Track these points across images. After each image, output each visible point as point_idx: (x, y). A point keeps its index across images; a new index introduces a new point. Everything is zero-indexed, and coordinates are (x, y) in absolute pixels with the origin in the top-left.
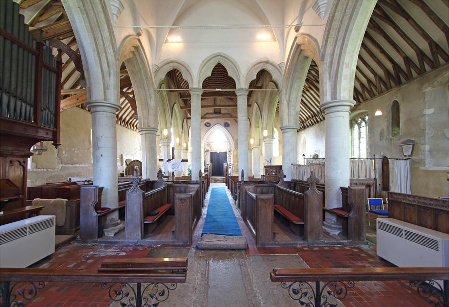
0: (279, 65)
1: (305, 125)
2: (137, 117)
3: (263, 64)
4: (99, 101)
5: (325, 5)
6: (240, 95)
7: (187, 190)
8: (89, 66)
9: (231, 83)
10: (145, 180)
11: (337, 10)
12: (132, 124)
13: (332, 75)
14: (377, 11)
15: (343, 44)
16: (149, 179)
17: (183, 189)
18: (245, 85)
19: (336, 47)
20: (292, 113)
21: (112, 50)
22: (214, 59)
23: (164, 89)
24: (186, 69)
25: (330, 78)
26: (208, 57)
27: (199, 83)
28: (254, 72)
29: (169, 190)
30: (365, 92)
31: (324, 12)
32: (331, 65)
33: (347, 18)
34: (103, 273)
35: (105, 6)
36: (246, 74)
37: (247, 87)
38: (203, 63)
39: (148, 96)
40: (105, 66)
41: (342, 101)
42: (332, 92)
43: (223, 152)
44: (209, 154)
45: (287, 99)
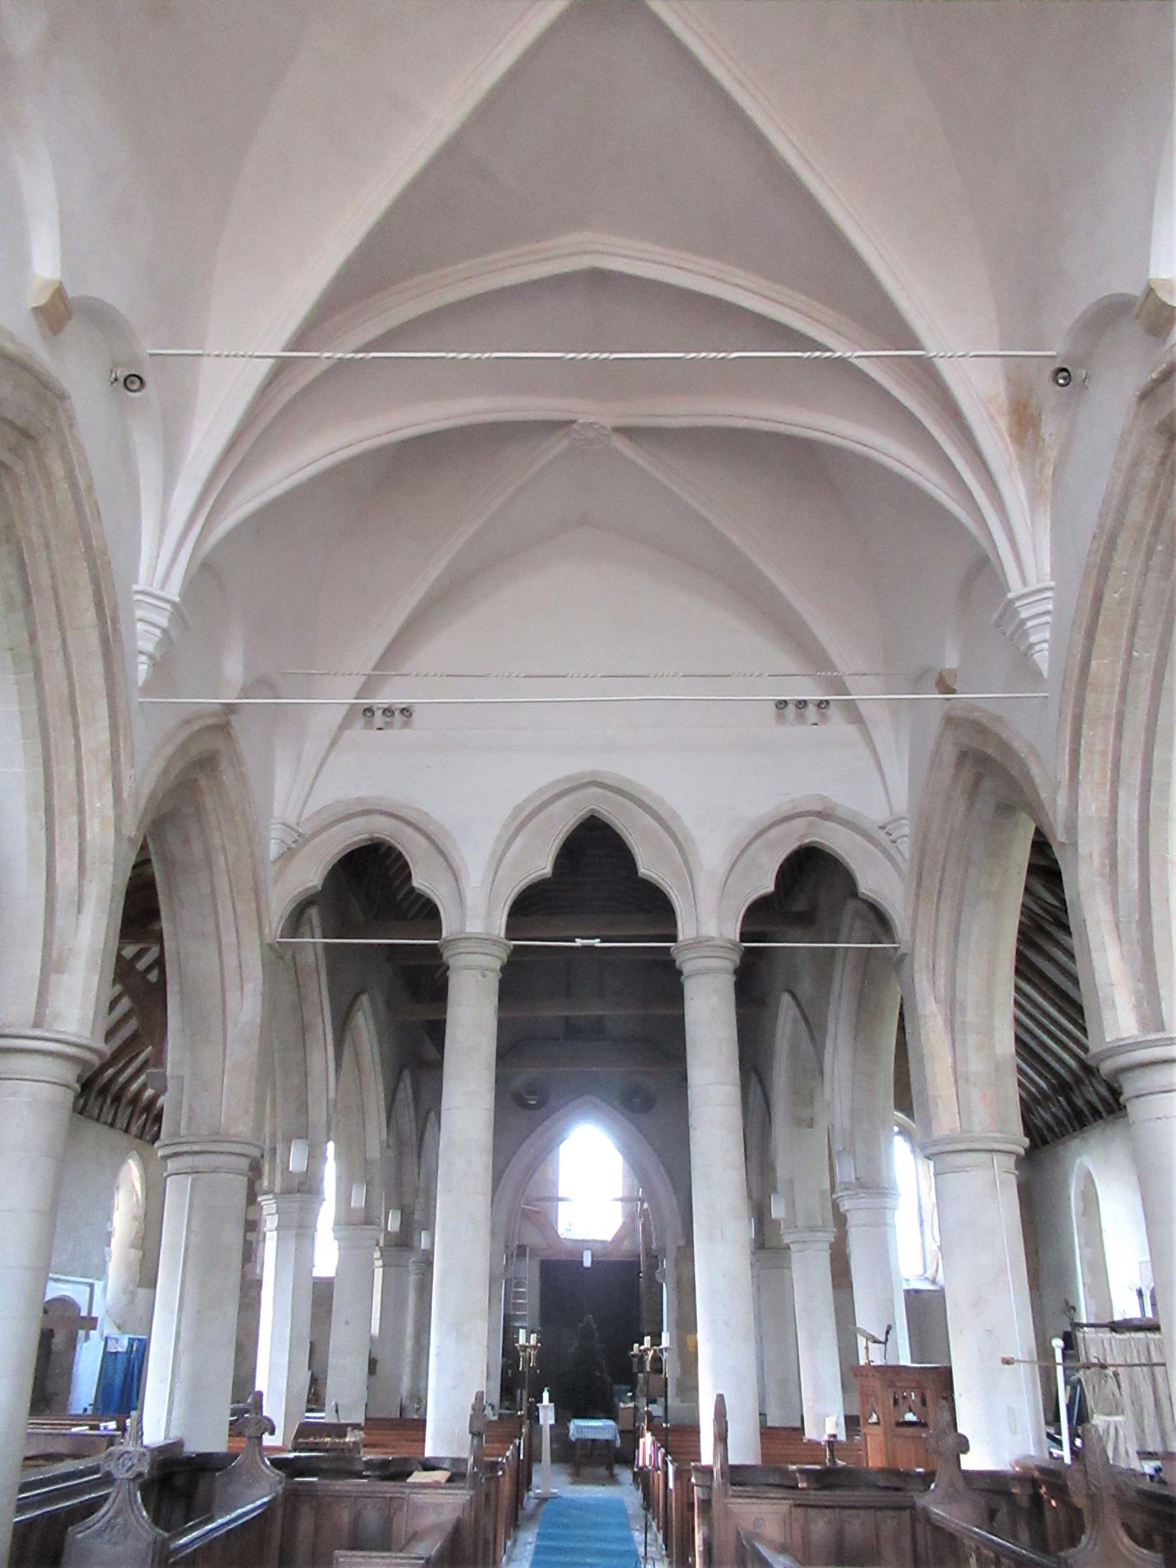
1: (1079, 1102)
2: (164, 1077)
3: (805, 820)
4: (13, 1031)
5: (1047, 618)
6: (697, 973)
7: (401, 1526)
10: (161, 1449)
11: (1095, 648)
12: (114, 1088)
13: (1122, 912)
15: (1146, 784)
16: (179, 1444)
17: (372, 1517)
19: (1122, 793)
20: (976, 1064)
21: (109, 800)
23: (314, 941)
25: (1117, 925)
27: (489, 914)
29: (292, 1517)
31: (1045, 645)
32: (1114, 865)
33: (1145, 679)
34: (1056, 1043)
35: (115, 630)
36: (722, 870)
37: (733, 931)
38: (513, 817)
40: (66, 866)
42: (1137, 991)
43: (614, 1263)
44: (530, 1272)
45: (942, 993)
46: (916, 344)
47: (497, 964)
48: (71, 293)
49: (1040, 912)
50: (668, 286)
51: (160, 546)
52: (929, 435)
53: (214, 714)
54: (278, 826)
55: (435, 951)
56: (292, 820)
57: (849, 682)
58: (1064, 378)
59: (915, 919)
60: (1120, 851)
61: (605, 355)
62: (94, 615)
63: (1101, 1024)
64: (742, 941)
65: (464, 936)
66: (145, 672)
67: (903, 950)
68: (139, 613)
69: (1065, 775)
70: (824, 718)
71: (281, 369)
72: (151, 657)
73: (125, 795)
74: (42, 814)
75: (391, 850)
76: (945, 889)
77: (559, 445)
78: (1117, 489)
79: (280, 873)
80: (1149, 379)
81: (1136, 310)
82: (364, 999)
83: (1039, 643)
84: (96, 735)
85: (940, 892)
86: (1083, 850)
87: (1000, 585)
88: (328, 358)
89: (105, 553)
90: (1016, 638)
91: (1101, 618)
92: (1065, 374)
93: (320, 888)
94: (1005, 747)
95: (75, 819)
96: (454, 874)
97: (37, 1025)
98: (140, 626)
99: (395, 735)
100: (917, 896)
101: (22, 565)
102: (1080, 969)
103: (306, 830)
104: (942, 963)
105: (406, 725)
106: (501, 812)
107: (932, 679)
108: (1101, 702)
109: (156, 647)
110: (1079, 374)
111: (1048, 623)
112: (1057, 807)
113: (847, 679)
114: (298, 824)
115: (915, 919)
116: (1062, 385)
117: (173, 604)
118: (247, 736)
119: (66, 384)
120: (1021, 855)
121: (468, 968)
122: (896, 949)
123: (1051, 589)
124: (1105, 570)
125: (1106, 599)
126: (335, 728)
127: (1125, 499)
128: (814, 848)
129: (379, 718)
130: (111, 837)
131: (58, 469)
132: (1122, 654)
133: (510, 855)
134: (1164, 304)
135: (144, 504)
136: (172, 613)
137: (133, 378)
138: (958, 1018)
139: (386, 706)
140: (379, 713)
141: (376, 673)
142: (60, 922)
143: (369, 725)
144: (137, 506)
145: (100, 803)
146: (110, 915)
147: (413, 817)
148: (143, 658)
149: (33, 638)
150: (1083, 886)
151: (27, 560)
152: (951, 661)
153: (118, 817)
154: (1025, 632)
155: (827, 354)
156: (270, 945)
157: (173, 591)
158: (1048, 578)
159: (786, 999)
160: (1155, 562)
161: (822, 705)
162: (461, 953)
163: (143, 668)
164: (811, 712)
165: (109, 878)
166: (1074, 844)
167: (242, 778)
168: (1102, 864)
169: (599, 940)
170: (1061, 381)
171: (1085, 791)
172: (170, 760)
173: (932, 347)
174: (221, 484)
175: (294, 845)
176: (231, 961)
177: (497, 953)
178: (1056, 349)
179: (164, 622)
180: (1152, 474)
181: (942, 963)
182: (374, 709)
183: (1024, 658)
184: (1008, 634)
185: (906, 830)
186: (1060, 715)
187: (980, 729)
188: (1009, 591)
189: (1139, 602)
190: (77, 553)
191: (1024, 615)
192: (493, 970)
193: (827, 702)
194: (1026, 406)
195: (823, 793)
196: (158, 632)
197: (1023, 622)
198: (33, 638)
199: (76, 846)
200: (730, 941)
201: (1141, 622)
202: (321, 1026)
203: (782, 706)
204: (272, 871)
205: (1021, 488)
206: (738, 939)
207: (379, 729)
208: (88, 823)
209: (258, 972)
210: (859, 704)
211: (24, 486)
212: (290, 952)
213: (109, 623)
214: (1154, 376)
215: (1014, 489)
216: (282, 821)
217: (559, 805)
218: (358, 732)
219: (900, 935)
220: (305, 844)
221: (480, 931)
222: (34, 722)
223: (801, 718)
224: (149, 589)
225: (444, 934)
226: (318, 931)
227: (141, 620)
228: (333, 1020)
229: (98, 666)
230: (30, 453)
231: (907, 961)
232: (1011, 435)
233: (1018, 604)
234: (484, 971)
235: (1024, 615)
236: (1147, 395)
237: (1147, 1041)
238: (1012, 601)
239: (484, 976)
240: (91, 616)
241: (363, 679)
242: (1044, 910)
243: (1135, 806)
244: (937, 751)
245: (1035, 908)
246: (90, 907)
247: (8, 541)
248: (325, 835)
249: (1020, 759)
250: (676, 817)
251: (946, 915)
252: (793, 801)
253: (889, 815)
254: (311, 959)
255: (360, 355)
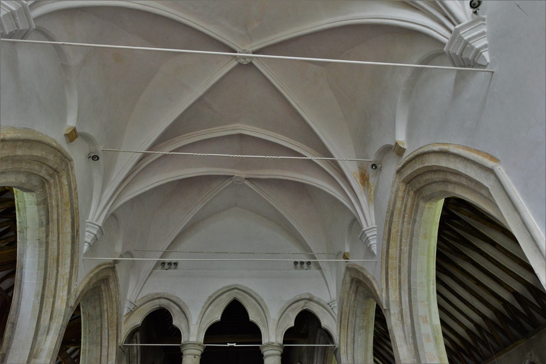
0: (328, 304)
3: (304, 301)
5: (375, 237)
8: (20, 319)
19: (402, 292)
21: (66, 293)
22: (226, 294)
24: (181, 308)
26: (218, 291)
27: (199, 333)
30: (479, 344)
35: (77, 234)
36: (277, 318)
37: (280, 340)
38: (208, 300)
47: (199, 353)
48: (78, 130)
49: (378, 332)
50: (261, 139)
54: (128, 303)
55: (179, 348)
56: (133, 301)
57: (316, 256)
58: (375, 167)
59: (340, 336)
60: (404, 312)
61: (242, 156)
62: (71, 229)
66: (86, 249)
67: (336, 347)
68: (87, 229)
69: (384, 286)
70: (309, 268)
71: (145, 156)
72: (89, 244)
73: (72, 291)
74: (39, 298)
75: (168, 312)
76: (349, 325)
77: (228, 183)
78: (393, 198)
80: (399, 167)
81: (393, 148)
83: (373, 244)
84: (65, 270)
85: (348, 326)
86: (392, 312)
87: (361, 227)
88: (161, 154)
89: (77, 209)
90: (362, 238)
91: (391, 237)
92: (375, 166)
93: (140, 325)
94: (365, 277)
95: (52, 300)
99: (171, 272)
100: (340, 327)
101: (48, 212)
102: (395, 354)
103: (138, 304)
104: (350, 351)
105: (175, 268)
107: (342, 255)
108: (393, 263)
110: (379, 166)
111: (375, 238)
112: (383, 297)
114: (135, 302)
116: (374, 169)
117: (100, 227)
118: (121, 272)
120: (373, 314)
121: (189, 354)
122: (334, 346)
123: (376, 228)
124: (391, 222)
125: (392, 231)
126: (152, 268)
128: (307, 311)
129: (166, 266)
132: (398, 248)
134: (401, 148)
135: (94, 195)
136: (98, 229)
137: (95, 156)
139: (169, 262)
140: (166, 265)
141: (166, 251)
142: (39, 338)
143: (163, 268)
145: (62, 294)
146: (59, 335)
148: (86, 244)
149: (47, 236)
150: (393, 324)
152: (347, 250)
153: (68, 299)
154: (369, 241)
156: (120, 347)
157: (100, 223)
158: (374, 224)
161: (309, 263)
162: (187, 349)
163: (86, 247)
164: (305, 265)
166: (389, 310)
167: (117, 286)
168: (398, 316)
169: (235, 344)
170: (374, 168)
172: (91, 278)
173: (337, 158)
175: (133, 310)
176: (104, 353)
177: (201, 349)
178: (372, 159)
179: (95, 232)
180: (402, 194)
182: (165, 263)
183: (369, 248)
184: (364, 241)
185: (336, 305)
186: (381, 267)
187: (358, 272)
188: (363, 228)
190: (68, 208)
191: (368, 235)
192: (198, 355)
194: (364, 175)
196: (93, 235)
197: (368, 238)
198: (47, 236)
199: (51, 310)
200: (279, 344)
201: (403, 238)
203: (302, 264)
206: (282, 343)
207: (166, 269)
208: (56, 301)
209: (114, 357)
211: (52, 187)
212: (127, 349)
213: (75, 232)
214: (400, 166)
215: (363, 199)
216: (130, 301)
217: (224, 296)
218: (159, 270)
219: (336, 342)
221: (194, 341)
222: (42, 265)
223: (302, 268)
225: (182, 342)
226: (138, 341)
229: (69, 246)
230: (57, 177)
231: (338, 350)
232: (361, 183)
233: (366, 232)
235: (368, 235)
236: (399, 172)
238: (364, 232)
239: (195, 358)
240: (69, 229)
242: (380, 332)
246: (52, 332)
249: (370, 281)
250: (262, 300)
253: (330, 300)
254: (135, 351)
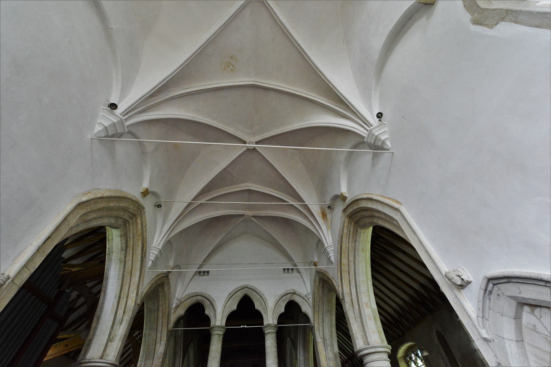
0: (306, 296)
3: (290, 294)
5: (333, 251)
9: (258, 317)
14: (337, 312)
15: (356, 285)
18: (273, 319)
19: (352, 287)
21: (135, 295)
22: (241, 291)
26: (235, 289)
28: (282, 304)
36: (273, 307)
37: (275, 322)
38: (229, 296)
39: (158, 340)
40: (120, 312)
41: (375, 347)
46: (304, 202)
51: (159, 238)
52: (308, 217)
53: (165, 273)
56: (179, 298)
59: (314, 318)
60: (353, 300)
63: (355, 343)
64: (278, 325)
65: (215, 326)
69: (340, 284)
71: (190, 204)
72: (152, 261)
75: (202, 305)
78: (341, 227)
79: (174, 312)
81: (340, 197)
82: (192, 344)
84: (136, 279)
86: (346, 300)
87: (323, 245)
96: (215, 310)
97: (101, 358)
98: (151, 254)
99: (205, 277)
102: (354, 345)
103: (182, 300)
104: (321, 329)
105: (208, 275)
106: (226, 295)
107: (313, 263)
108: (345, 268)
109: (154, 259)
110: (332, 207)
112: (339, 290)
113: (297, 264)
114: (181, 299)
115: (314, 318)
119: (145, 206)
120: (334, 302)
122: (311, 325)
124: (342, 241)
127: (343, 229)
129: (202, 274)
130: (133, 304)
131: (139, 221)
132: (347, 258)
133: (227, 305)
134: (344, 196)
138: (325, 343)
140: (202, 273)
142: (115, 327)
143: (200, 275)
144: (156, 228)
145: (133, 296)
147: (207, 296)
148: (150, 261)
149: (125, 257)
150: (347, 309)
151: (128, 240)
152: (316, 260)
153: (136, 299)
155: (289, 203)
156: (170, 331)
157: (160, 247)
159: (288, 339)
160: (350, 240)
161: (292, 269)
163: (150, 263)
165: (130, 315)
166: (344, 299)
167: (169, 288)
169: (246, 326)
171: (344, 287)
173: (307, 203)
174: (175, 225)
178: (328, 203)
179: (157, 253)
181: (321, 329)
183: (329, 259)
184: (326, 254)
189: (349, 248)
191: (328, 250)
192: (221, 335)
193: (293, 268)
194: (324, 213)
195: (294, 288)
196: (155, 255)
197: (328, 252)
198: (125, 257)
200: (275, 325)
201: (350, 252)
202: (180, 352)
204: (173, 311)
205: (325, 227)
206: (277, 324)
207: (202, 276)
208: (128, 301)
209: (165, 338)
210: (299, 269)
211: (131, 225)
213: (144, 253)
214: (345, 207)
215: (324, 227)
217: (239, 293)
220: (182, 304)
222: (121, 276)
223: (288, 272)
224: (155, 246)
227: (151, 253)
228: (183, 350)
229: (139, 263)
234: (219, 335)
235: (328, 250)
236: (344, 211)
237: (366, 348)
239: (219, 337)
240: (140, 252)
241: (199, 265)
243: (355, 289)
244: (315, 279)
245: (338, 313)
247: (125, 236)
248: (186, 301)
251: (321, 317)
252: (287, 290)
255: (207, 202)
